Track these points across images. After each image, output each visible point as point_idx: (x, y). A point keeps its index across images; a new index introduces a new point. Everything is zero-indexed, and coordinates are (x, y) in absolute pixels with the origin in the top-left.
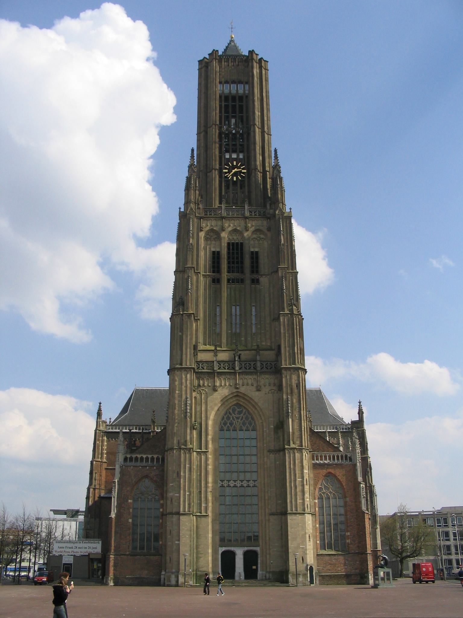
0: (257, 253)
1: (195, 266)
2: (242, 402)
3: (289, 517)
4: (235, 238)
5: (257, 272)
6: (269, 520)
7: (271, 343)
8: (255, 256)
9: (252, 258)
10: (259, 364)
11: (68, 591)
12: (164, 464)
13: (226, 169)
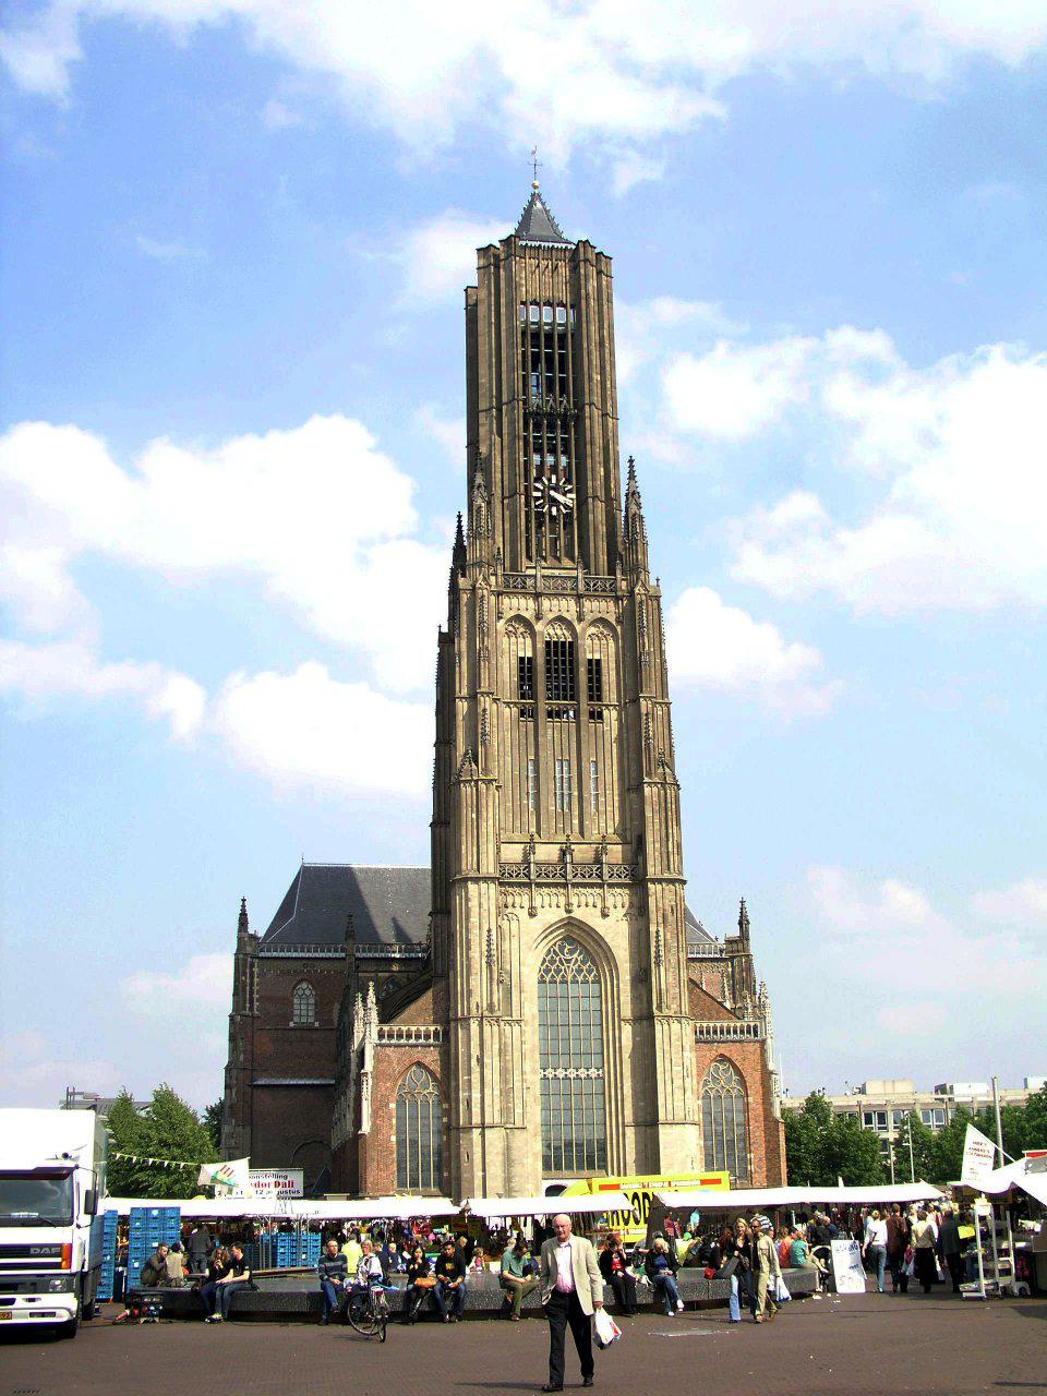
0: (598, 662)
4: (559, 632)
5: (599, 698)
8: (595, 667)
9: (590, 672)
10: (605, 869)
11: (950, 1192)
12: (449, 1042)
13: (537, 489)
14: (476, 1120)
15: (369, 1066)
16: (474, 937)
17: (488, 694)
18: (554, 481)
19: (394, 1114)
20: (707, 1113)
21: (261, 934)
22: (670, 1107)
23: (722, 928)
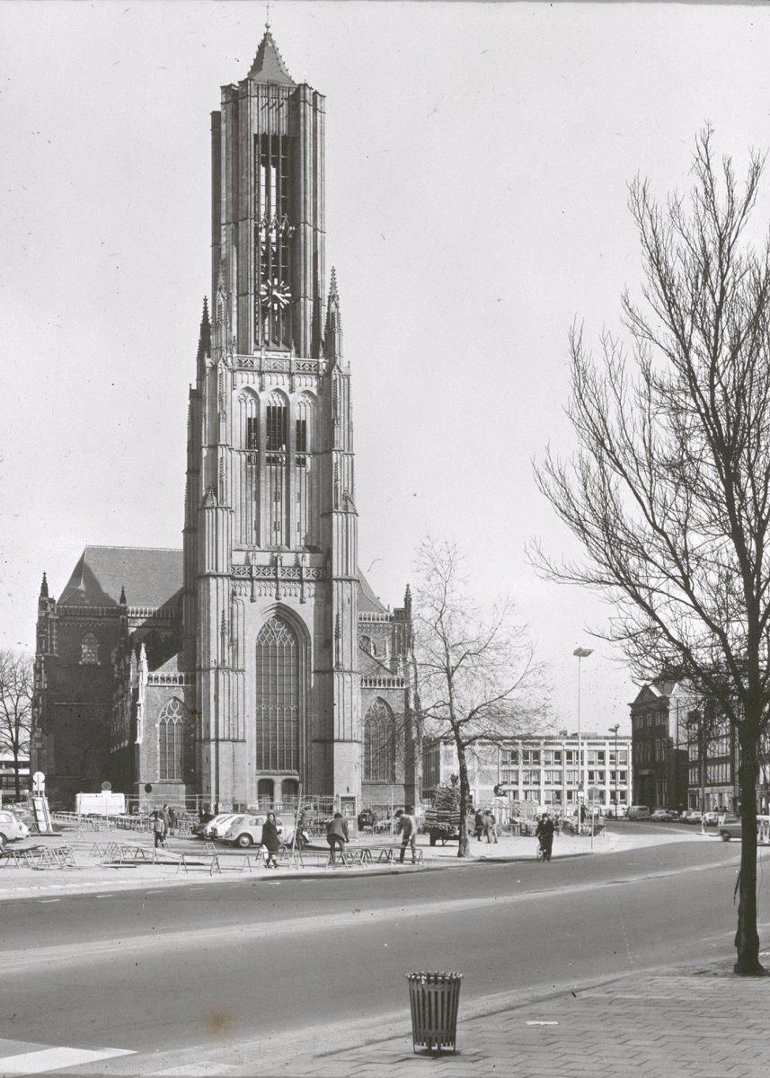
1: (229, 443)
3: (336, 746)
7: (318, 543)
14: (213, 736)
15: (141, 700)
16: (213, 615)
17: (225, 446)
18: (276, 283)
19: (158, 731)
20: (367, 735)
21: (57, 599)
22: (342, 731)
23: (395, 602)
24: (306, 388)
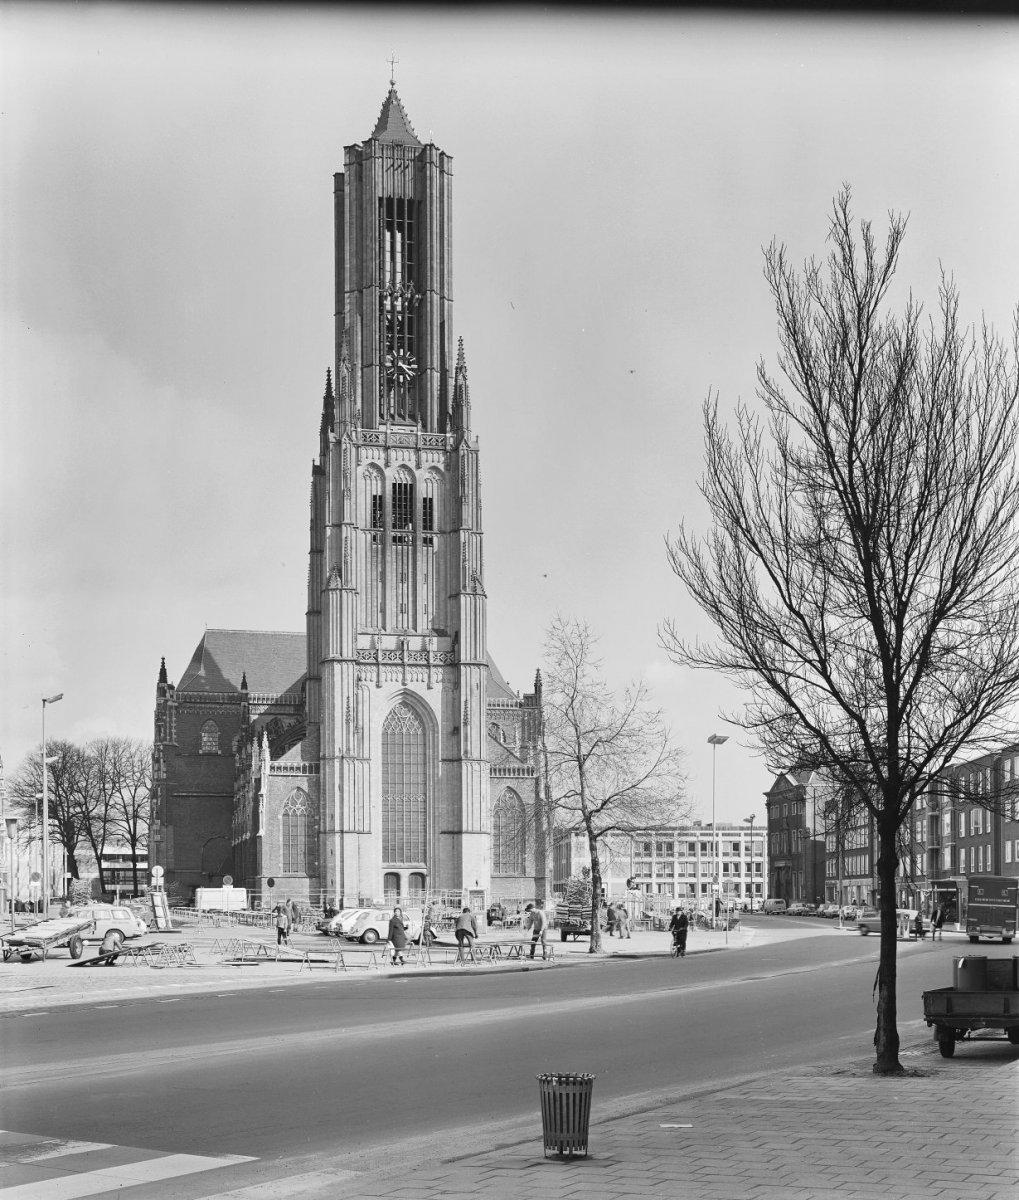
2: (410, 700)
6: (439, 839)
7: (446, 626)
8: (428, 503)
24: (433, 464)
